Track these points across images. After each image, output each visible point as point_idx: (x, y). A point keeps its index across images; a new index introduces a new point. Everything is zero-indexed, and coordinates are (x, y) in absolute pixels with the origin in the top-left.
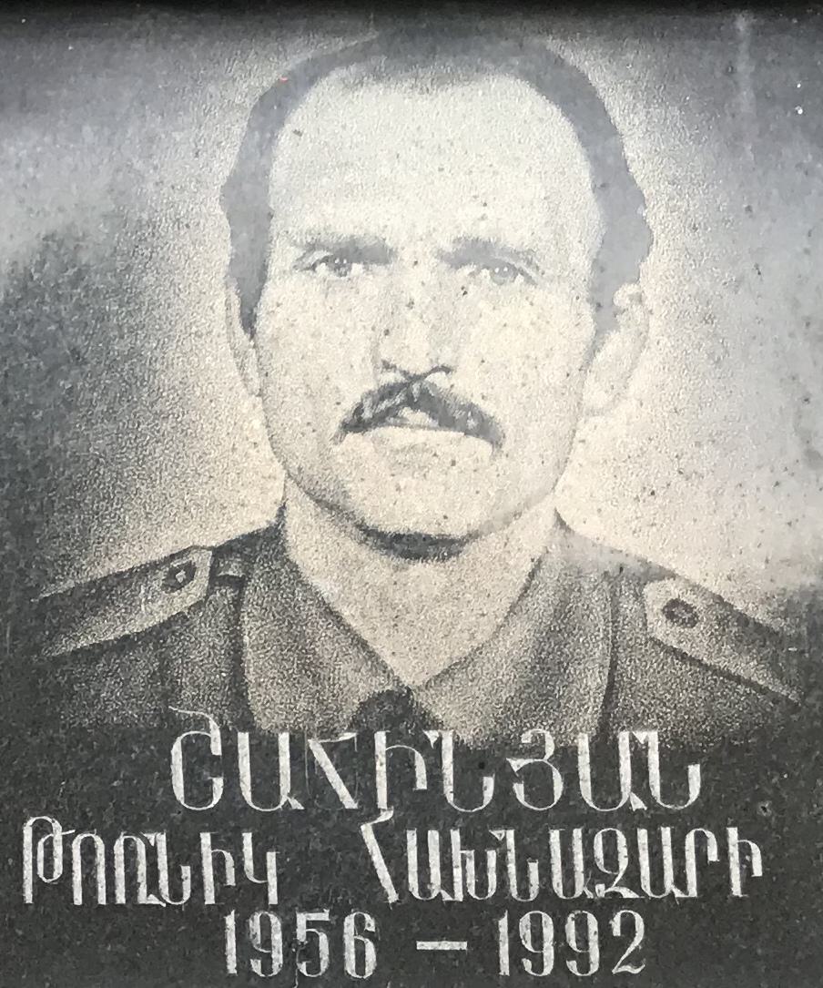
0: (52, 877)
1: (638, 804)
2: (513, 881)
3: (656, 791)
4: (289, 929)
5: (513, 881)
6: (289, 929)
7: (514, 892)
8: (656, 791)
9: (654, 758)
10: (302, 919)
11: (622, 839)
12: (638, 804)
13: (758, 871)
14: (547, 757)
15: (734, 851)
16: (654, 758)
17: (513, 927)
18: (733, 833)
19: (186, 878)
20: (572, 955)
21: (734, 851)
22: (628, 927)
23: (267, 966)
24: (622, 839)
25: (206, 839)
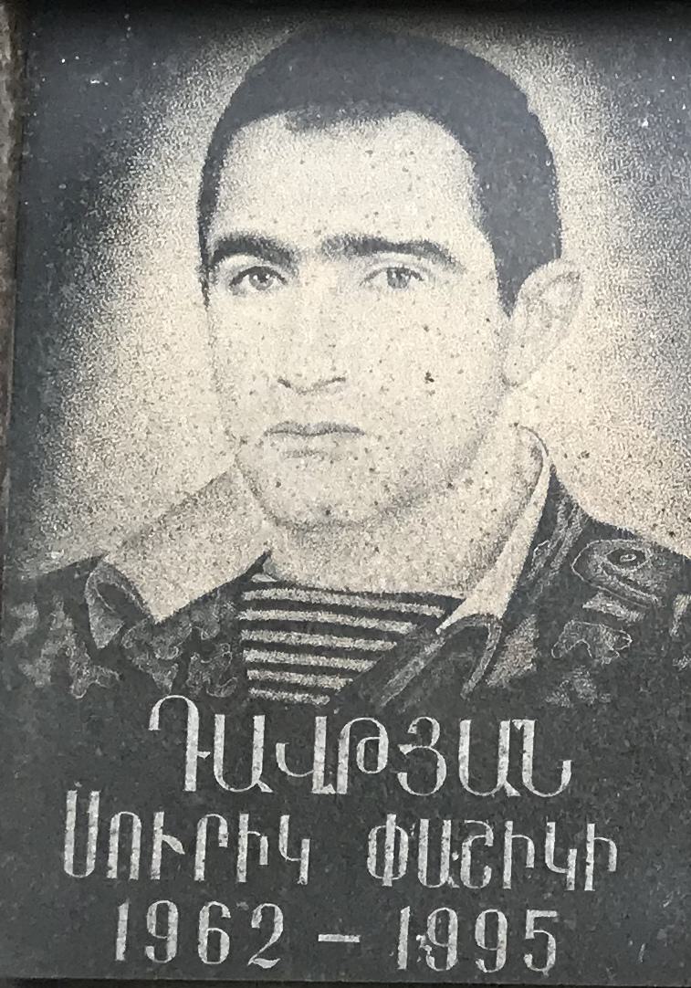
0: (209, 818)
1: (513, 792)
2: (423, 863)
3: (527, 778)
4: (517, 926)
5: (423, 863)
6: (517, 926)
7: (423, 877)
8: (527, 778)
9: (529, 745)
10: (531, 915)
11: (137, 823)
12: (513, 792)
13: (613, 867)
14: (432, 744)
15: (244, 842)
16: (529, 745)
17: (417, 926)
18: (244, 819)
19: (115, 832)
20: (150, 940)
21: (244, 842)
22: (268, 916)
23: (161, 953)
24: (137, 823)
25: (591, 827)
